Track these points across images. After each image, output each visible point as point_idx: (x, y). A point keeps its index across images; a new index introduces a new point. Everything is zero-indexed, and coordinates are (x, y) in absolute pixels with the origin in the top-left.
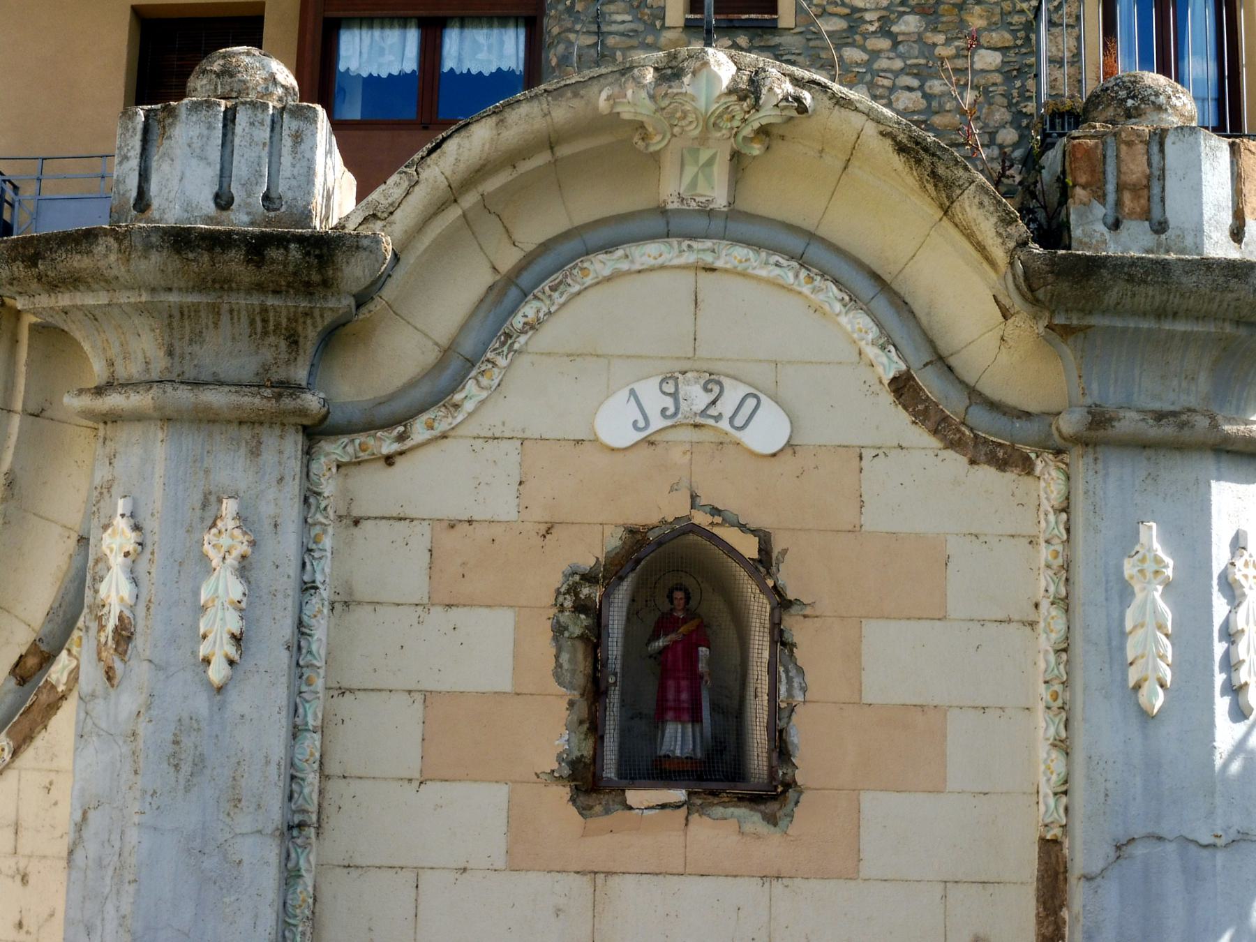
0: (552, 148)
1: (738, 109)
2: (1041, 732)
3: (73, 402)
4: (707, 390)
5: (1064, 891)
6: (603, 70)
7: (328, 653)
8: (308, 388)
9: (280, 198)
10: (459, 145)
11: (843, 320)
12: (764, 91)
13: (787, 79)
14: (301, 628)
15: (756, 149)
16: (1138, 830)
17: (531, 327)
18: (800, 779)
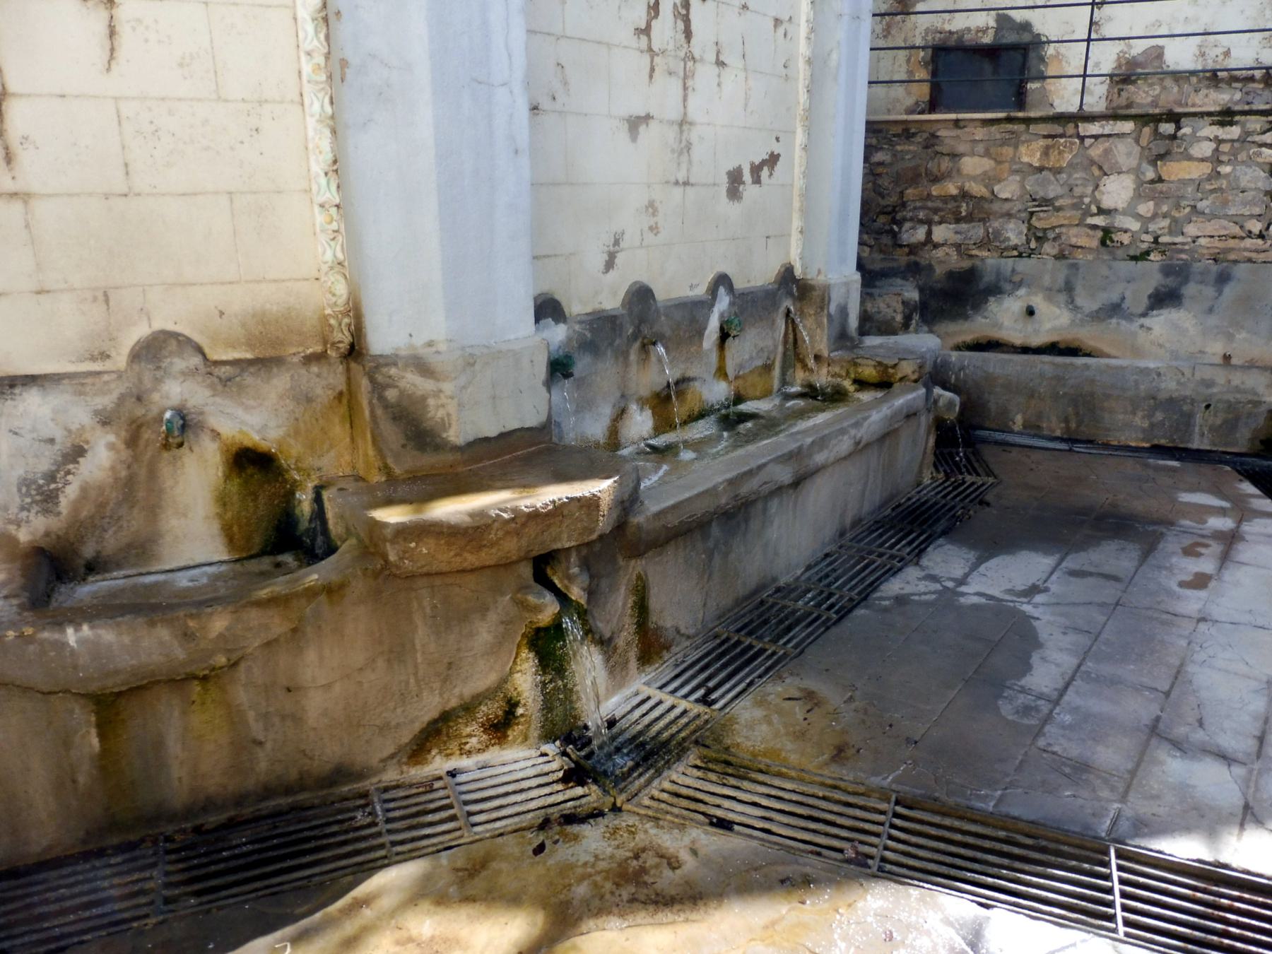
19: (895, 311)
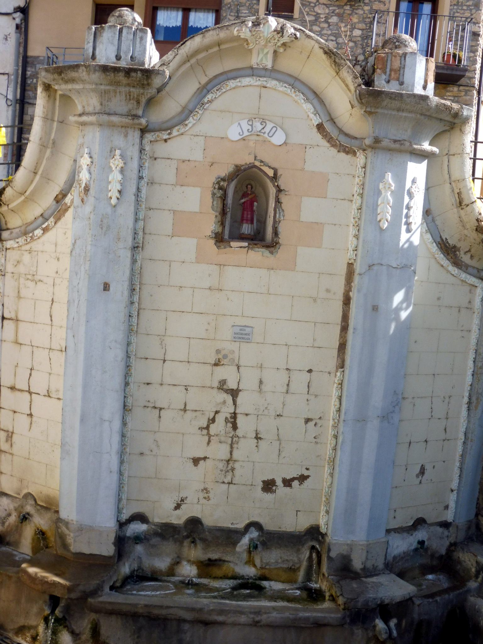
0: (219, 46)
1: (277, 37)
2: (351, 233)
3: (72, 119)
4: (261, 124)
5: (353, 278)
6: (236, 22)
7: (146, 198)
8: (143, 117)
9: (136, 57)
10: (191, 43)
11: (304, 105)
12: (285, 31)
13: (292, 28)
14: (138, 190)
15: (281, 50)
16: (376, 262)
17: (210, 102)
18: (280, 242)
19: (472, 565)
